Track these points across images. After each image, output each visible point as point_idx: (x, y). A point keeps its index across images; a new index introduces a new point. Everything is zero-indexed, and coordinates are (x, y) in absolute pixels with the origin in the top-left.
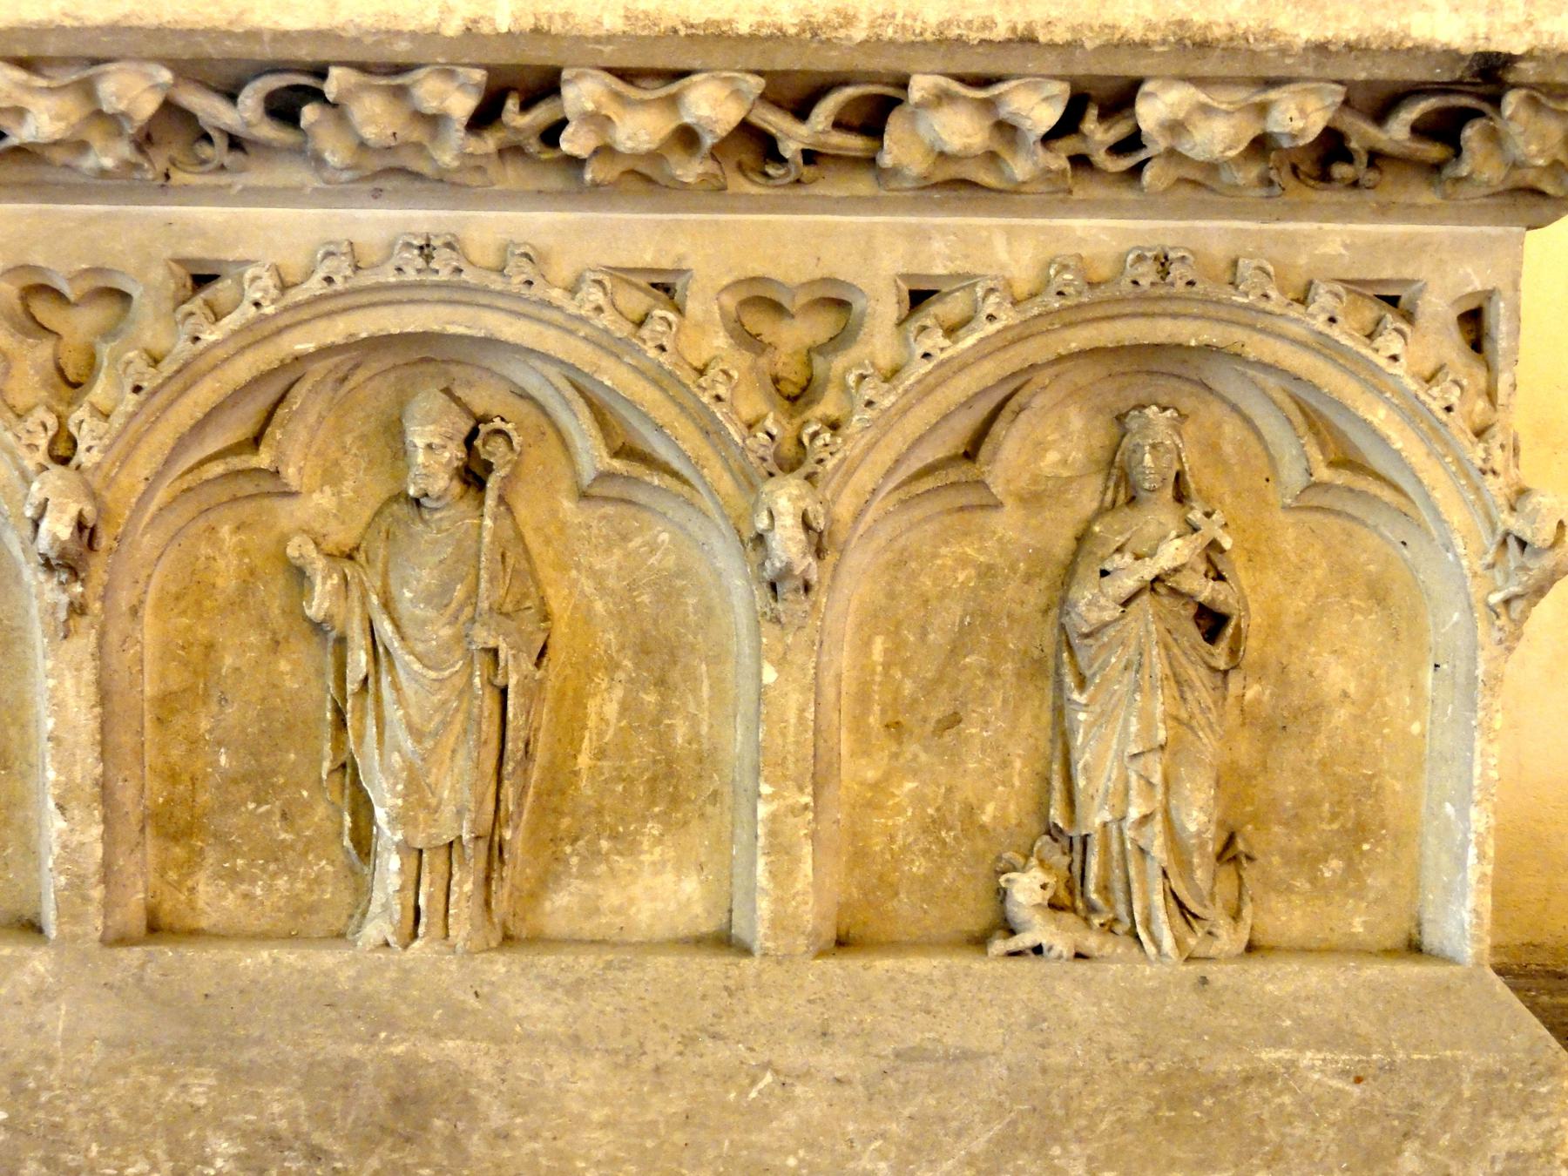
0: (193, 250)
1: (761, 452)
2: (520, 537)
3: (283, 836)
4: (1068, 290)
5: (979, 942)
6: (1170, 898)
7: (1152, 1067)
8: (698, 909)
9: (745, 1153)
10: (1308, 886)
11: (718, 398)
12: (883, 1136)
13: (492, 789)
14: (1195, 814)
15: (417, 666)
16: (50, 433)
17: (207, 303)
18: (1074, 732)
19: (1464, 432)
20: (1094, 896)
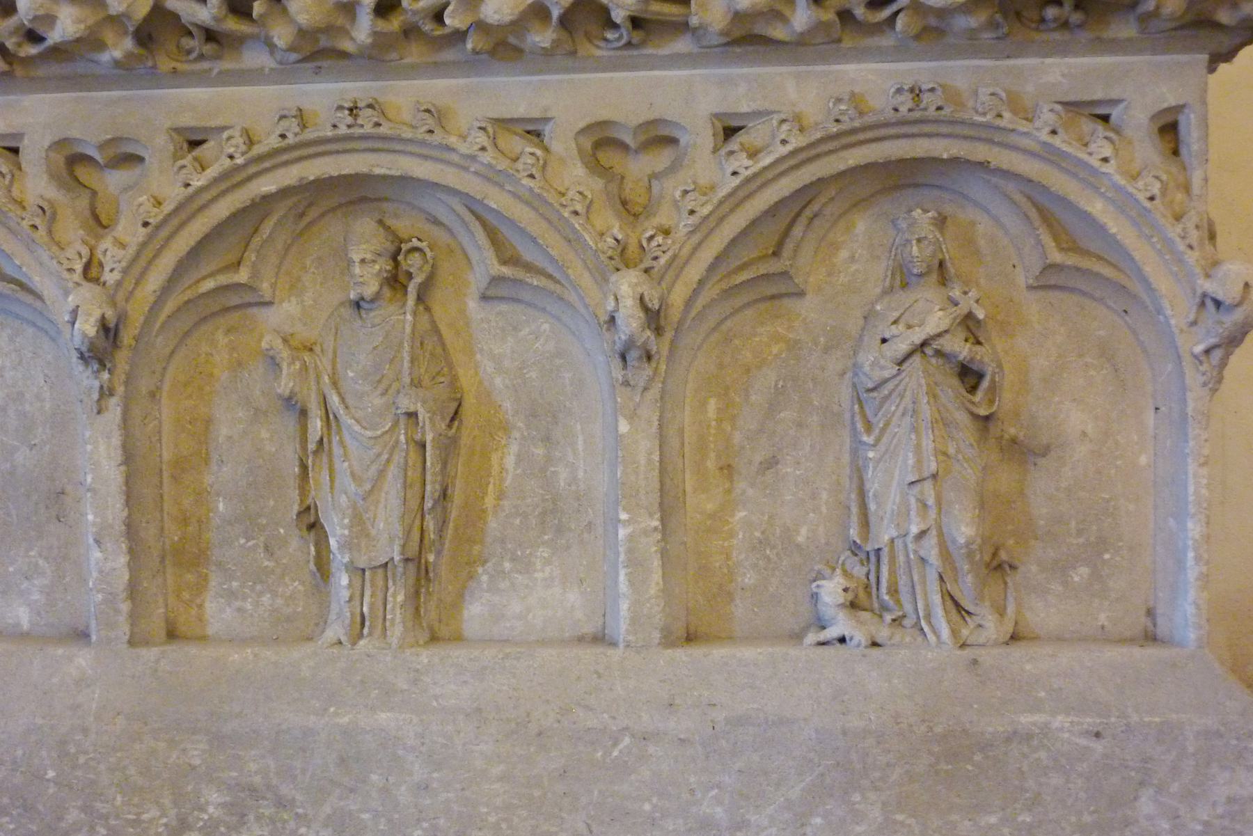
0: (187, 120)
1: (610, 253)
2: (436, 331)
3: (266, 563)
4: (844, 118)
5: (796, 637)
6: (947, 598)
7: (931, 729)
8: (579, 614)
9: (610, 800)
10: (1060, 588)
11: (576, 213)
12: (719, 786)
13: (418, 522)
14: (963, 529)
15: (357, 428)
16: (84, 260)
17: (196, 159)
18: (866, 467)
19: (1164, 216)
20: (886, 598)
